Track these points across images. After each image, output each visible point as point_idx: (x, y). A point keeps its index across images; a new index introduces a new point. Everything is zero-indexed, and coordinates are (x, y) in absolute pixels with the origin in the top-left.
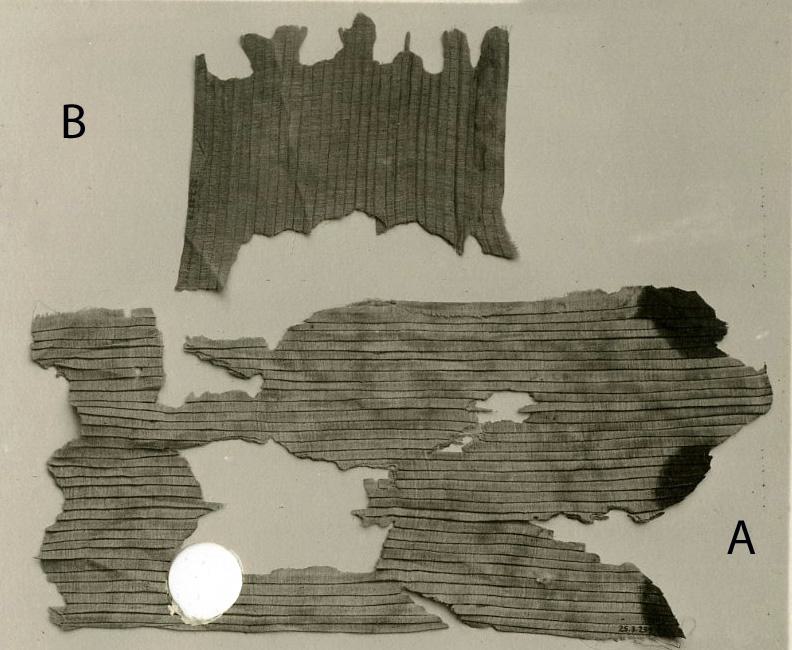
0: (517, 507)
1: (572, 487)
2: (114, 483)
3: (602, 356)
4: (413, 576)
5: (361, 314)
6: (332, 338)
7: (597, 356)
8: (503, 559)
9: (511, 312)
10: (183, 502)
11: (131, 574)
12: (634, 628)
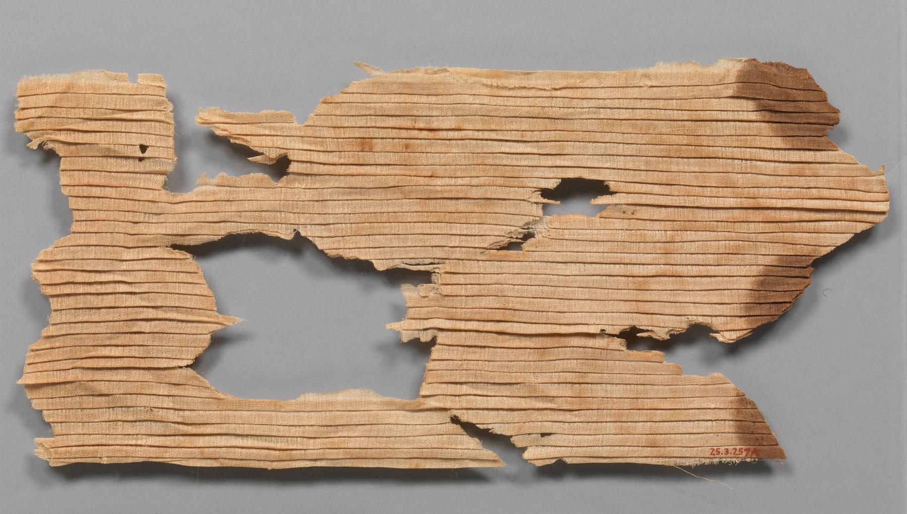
0: (578, 318)
1: (647, 296)
2: (110, 291)
3: (693, 140)
4: (464, 402)
5: (411, 84)
6: (372, 112)
7: (684, 140)
8: (570, 377)
9: (585, 85)
10: (193, 314)
11: (130, 400)
12: (727, 451)
